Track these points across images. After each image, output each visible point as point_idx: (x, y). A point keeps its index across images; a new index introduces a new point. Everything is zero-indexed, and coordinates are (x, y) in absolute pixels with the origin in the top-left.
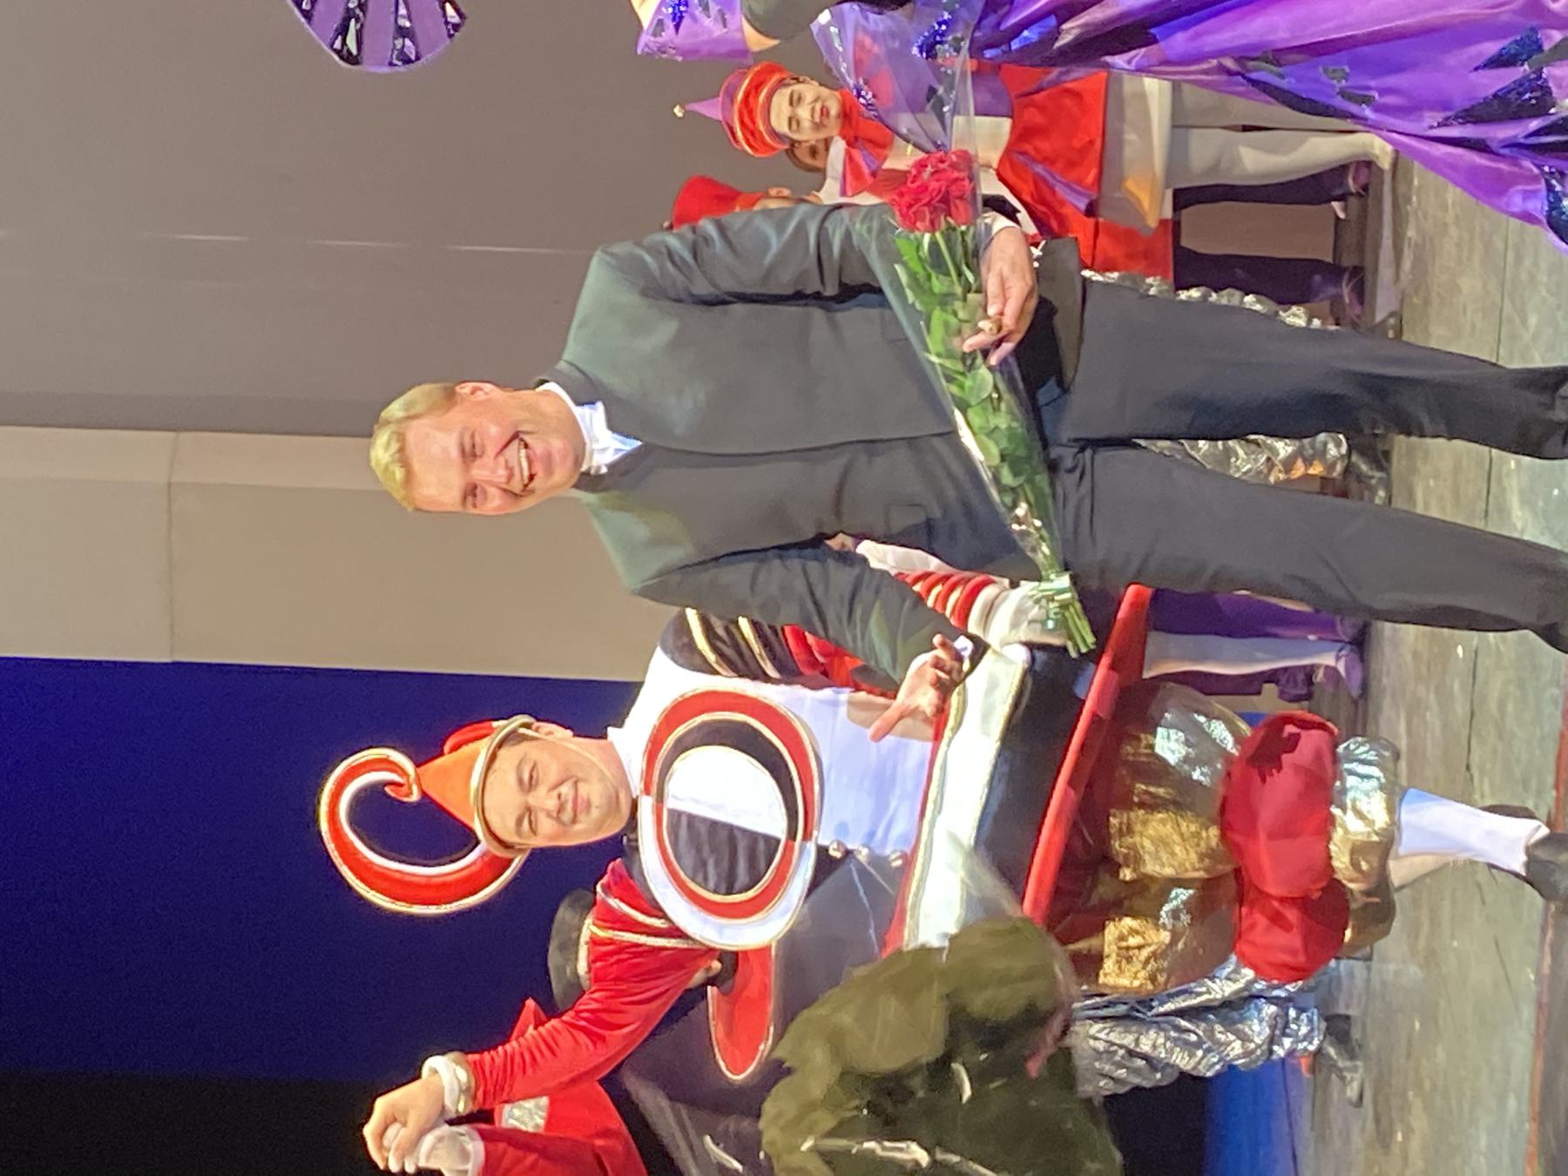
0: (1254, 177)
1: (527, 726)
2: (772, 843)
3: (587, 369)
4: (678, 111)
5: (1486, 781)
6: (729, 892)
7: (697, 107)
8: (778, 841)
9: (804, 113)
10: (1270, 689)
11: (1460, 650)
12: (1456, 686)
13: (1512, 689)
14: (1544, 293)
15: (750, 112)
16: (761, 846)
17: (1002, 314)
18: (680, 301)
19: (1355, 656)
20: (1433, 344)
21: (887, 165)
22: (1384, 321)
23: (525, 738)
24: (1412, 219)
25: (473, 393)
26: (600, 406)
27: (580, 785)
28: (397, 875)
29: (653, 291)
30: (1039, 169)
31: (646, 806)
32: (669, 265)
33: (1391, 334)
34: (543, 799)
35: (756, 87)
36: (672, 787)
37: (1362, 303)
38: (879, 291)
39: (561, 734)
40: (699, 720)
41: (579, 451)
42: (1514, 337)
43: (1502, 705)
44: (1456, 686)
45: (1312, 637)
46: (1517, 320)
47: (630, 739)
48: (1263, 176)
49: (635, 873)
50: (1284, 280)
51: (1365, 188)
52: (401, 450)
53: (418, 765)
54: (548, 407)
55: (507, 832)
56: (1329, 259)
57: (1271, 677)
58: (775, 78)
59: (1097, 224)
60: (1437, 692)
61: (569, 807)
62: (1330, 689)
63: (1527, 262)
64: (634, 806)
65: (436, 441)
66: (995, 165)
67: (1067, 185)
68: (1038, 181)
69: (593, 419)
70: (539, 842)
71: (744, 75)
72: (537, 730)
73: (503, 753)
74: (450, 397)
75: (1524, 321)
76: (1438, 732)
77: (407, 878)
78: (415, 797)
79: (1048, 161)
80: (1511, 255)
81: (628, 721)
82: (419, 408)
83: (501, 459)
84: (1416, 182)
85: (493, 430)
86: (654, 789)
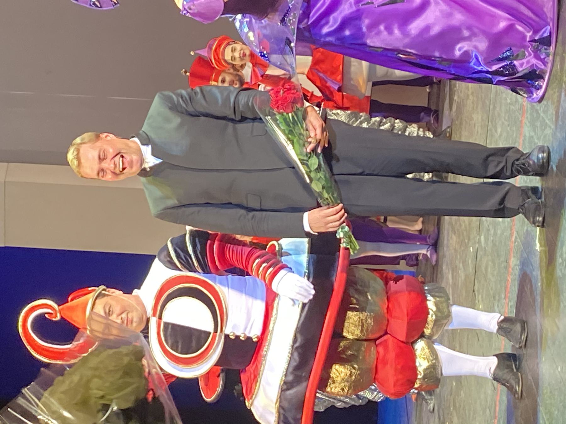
0: (399, 77)
1: (104, 290)
3: (148, 134)
4: (192, 53)
5: (480, 296)
7: (198, 52)
10: (403, 262)
11: (471, 249)
12: (470, 261)
13: (490, 263)
14: (503, 120)
15: (217, 55)
16: (203, 335)
17: (316, 135)
18: (182, 113)
19: (433, 251)
20: (463, 140)
21: (267, 73)
22: (446, 129)
23: (105, 295)
24: (456, 93)
25: (106, 137)
26: (150, 146)
29: (174, 108)
30: (321, 75)
31: (153, 322)
32: (180, 100)
33: (448, 135)
35: (219, 46)
37: (437, 123)
38: (261, 119)
39: (118, 293)
41: (142, 161)
42: (492, 136)
43: (486, 269)
44: (470, 261)
45: (418, 243)
50: (410, 114)
51: (440, 81)
52: (78, 154)
53: (59, 306)
54: (132, 145)
56: (427, 106)
57: (404, 257)
58: (226, 42)
59: (343, 95)
60: (463, 264)
61: (125, 322)
62: (424, 262)
63: (498, 109)
64: (148, 320)
65: (90, 154)
66: (306, 73)
67: (332, 81)
68: (321, 79)
69: (147, 150)
71: (215, 40)
72: (109, 292)
73: (97, 301)
74: (98, 137)
75: (496, 131)
76: (463, 278)
79: (324, 72)
80: (492, 107)
82: (86, 140)
83: (113, 161)
85: (111, 150)
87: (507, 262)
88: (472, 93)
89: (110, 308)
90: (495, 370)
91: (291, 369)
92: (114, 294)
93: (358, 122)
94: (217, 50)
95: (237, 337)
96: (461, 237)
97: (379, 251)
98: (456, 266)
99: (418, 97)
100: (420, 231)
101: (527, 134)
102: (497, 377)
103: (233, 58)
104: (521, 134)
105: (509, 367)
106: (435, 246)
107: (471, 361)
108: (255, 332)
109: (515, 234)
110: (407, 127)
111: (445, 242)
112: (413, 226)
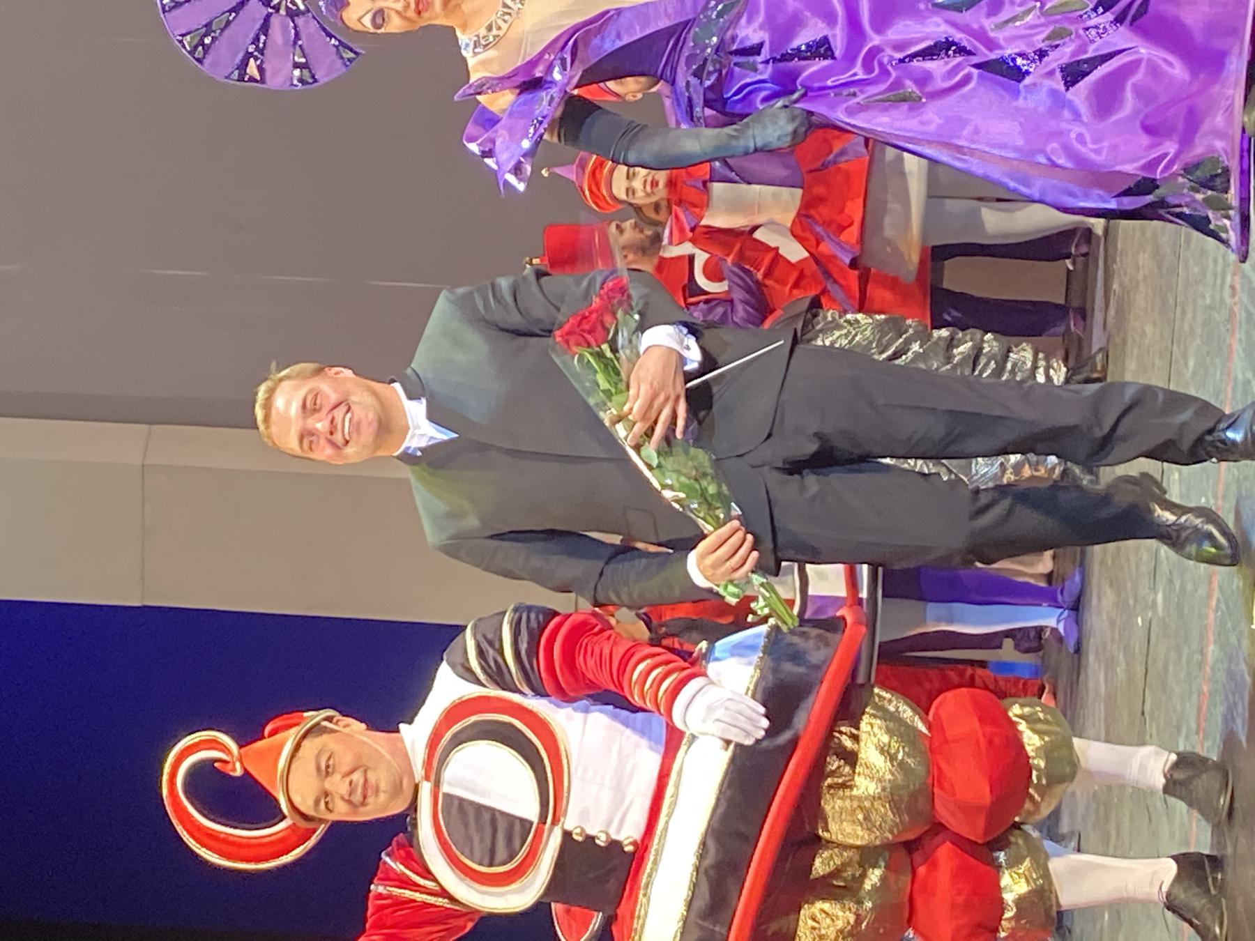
0: (995, 237)
1: (329, 719)
2: (525, 824)
4: (545, 173)
6: (491, 865)
7: (557, 170)
8: (531, 823)
9: (637, 184)
16: (517, 827)
21: (704, 222)
27: (369, 774)
28: (222, 836)
31: (426, 790)
34: (338, 785)
36: (448, 774)
39: (357, 726)
40: (474, 718)
43: (1166, 668)
46: (1182, 362)
47: (415, 734)
48: (1005, 236)
49: (415, 843)
53: (241, 747)
55: (306, 806)
56: (1062, 301)
57: (1009, 634)
61: (360, 790)
63: (1189, 316)
69: (416, 411)
70: (332, 817)
73: (306, 743)
75: (1186, 365)
77: (231, 838)
78: (238, 772)
81: (417, 719)
84: (1119, 247)
86: (433, 777)
87: (1202, 653)
88: (1145, 278)
89: (329, 759)
90: (1172, 885)
91: (693, 917)
92: (347, 730)
93: (901, 340)
94: (598, 176)
95: (591, 839)
96: (1123, 595)
97: (951, 621)
98: (1113, 657)
99: (1041, 283)
100: (1049, 577)
101: (1240, 377)
102: (1176, 903)
103: (630, 191)
104: (1229, 374)
105: (1201, 882)
106: (1077, 607)
107: (1118, 868)
108: (629, 832)
109: (1216, 594)
110: (1009, 351)
111: (1094, 601)
112: (1032, 564)
